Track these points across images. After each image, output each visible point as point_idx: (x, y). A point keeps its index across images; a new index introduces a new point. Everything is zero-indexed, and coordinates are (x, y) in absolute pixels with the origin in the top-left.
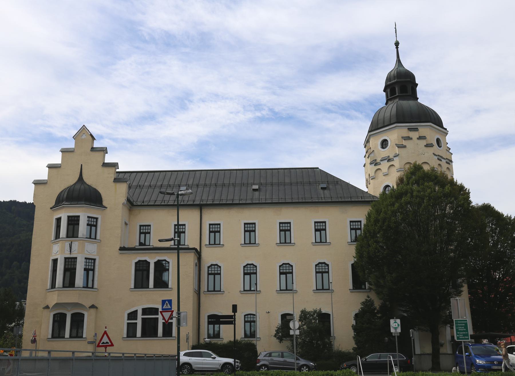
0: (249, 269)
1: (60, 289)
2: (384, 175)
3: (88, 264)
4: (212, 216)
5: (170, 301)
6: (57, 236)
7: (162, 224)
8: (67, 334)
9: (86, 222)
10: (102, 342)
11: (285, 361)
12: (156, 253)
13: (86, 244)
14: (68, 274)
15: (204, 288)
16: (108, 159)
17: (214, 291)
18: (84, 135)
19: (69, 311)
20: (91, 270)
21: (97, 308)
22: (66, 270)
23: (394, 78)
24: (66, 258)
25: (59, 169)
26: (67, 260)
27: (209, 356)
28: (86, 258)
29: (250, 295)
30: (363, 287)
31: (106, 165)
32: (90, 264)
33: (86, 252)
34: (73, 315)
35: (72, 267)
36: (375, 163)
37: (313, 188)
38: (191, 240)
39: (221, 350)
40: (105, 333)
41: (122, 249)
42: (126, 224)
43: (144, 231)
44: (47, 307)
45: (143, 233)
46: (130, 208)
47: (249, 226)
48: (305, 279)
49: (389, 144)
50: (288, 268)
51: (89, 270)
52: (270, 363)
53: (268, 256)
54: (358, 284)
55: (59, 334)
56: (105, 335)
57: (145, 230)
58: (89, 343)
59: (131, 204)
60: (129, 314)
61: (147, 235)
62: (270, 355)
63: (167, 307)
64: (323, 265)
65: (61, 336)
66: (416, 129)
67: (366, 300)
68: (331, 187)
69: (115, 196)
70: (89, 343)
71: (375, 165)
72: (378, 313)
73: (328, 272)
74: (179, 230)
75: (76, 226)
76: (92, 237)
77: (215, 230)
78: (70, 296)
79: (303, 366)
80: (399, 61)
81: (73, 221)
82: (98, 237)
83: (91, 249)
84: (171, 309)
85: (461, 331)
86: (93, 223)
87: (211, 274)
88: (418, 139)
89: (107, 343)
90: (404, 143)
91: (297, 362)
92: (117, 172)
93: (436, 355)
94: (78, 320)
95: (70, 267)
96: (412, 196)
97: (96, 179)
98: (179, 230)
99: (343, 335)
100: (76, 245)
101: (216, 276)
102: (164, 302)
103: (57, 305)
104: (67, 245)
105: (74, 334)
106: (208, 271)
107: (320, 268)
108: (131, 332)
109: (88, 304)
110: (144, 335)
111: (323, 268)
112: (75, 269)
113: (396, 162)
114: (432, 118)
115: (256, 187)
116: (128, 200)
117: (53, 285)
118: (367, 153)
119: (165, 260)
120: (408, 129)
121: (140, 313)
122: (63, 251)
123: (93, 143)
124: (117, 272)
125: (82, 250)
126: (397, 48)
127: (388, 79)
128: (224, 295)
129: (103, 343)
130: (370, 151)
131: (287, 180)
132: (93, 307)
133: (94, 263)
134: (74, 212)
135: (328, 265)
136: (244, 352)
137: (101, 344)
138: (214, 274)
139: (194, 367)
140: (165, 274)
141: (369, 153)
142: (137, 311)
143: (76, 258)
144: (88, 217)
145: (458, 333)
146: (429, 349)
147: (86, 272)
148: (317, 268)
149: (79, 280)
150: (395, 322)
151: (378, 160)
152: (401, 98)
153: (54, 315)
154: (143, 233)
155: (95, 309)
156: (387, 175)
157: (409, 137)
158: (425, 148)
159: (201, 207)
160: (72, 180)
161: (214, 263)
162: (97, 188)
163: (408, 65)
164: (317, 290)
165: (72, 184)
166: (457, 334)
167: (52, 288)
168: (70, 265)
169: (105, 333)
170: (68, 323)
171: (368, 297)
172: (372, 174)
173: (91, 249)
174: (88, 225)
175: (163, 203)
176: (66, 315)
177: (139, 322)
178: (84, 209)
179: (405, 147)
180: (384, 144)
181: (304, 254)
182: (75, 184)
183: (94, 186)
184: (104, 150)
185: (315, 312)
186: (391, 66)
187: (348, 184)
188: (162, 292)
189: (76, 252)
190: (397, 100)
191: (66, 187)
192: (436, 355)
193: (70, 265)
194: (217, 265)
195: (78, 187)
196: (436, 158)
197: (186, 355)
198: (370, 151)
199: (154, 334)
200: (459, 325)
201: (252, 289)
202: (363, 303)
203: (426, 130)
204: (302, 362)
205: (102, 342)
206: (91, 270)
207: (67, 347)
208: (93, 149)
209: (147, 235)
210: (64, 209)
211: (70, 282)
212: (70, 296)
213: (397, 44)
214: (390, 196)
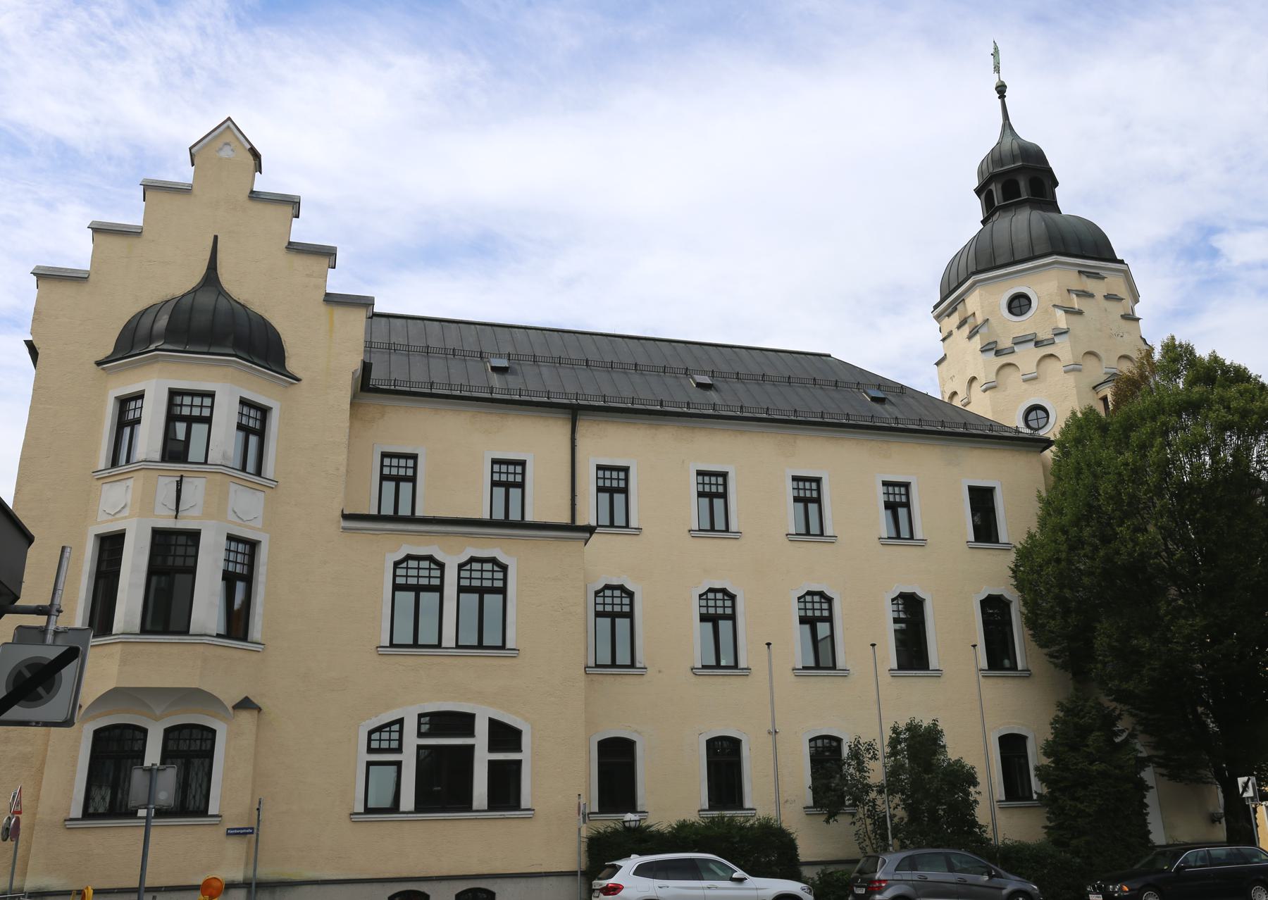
1: (132, 639)
2: (1025, 381)
4: (605, 444)
7: (457, 457)
11: (963, 883)
13: (233, 487)
18: (227, 148)
19: (157, 719)
21: (259, 709)
23: (1014, 158)
24: (156, 532)
29: (721, 680)
30: (1007, 663)
33: (232, 517)
38: (545, 500)
49: (1034, 304)
51: (239, 579)
53: (767, 570)
57: (400, 470)
58: (233, 833)
70: (233, 833)
74: (509, 476)
76: (252, 461)
77: (614, 483)
78: (166, 665)
81: (185, 412)
86: (255, 422)
94: (192, 749)
98: (509, 476)
103: (116, 696)
104: (166, 486)
109: (230, 696)
113: (1063, 348)
114: (1090, 247)
120: (1080, 272)
121: (411, 727)
124: (328, 590)
125: (216, 510)
126: (1002, 96)
128: (644, 678)
132: (246, 704)
134: (193, 374)
142: (490, 719)
147: (807, 627)
149: (207, 606)
151: (1005, 343)
153: (98, 734)
155: (256, 712)
156: (1035, 379)
158: (1123, 322)
159: (574, 412)
160: (181, 279)
162: (267, 316)
163: (1028, 133)
168: (173, 553)
173: (245, 509)
174: (701, 495)
176: (144, 731)
179: (1080, 313)
180: (1019, 304)
182: (194, 291)
183: (257, 307)
186: (988, 139)
189: (195, 512)
193: (173, 553)
199: (459, 799)
208: (254, 196)
210: (157, 366)
211: (166, 612)
212: (166, 665)
213: (1001, 90)
214: (1084, 428)
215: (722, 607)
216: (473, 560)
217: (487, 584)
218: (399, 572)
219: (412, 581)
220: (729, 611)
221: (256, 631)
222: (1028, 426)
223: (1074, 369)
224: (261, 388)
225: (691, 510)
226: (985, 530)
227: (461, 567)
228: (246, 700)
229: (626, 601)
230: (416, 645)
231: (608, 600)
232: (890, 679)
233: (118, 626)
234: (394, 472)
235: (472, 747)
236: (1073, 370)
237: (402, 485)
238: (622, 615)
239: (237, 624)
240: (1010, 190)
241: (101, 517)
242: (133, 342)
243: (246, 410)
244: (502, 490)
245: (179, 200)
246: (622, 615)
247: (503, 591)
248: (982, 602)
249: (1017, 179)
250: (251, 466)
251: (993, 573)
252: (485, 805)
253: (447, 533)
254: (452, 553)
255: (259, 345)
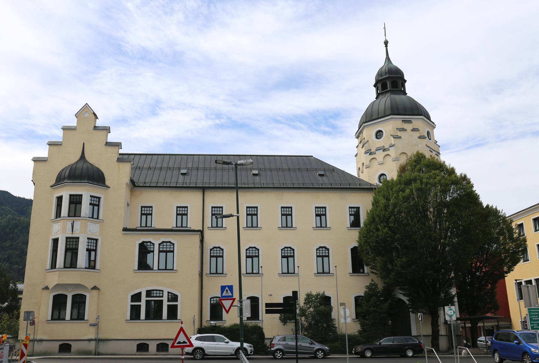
0: (251, 252)
2: (379, 164)
3: (90, 244)
5: (231, 288)
6: (58, 214)
7: (164, 207)
8: (68, 317)
9: (89, 202)
10: (177, 341)
12: (160, 234)
13: (89, 223)
14: (69, 254)
15: (206, 270)
16: (112, 138)
17: (217, 273)
19: (70, 292)
20: (93, 250)
21: (99, 289)
22: (67, 250)
23: (386, 73)
24: (67, 238)
25: (59, 147)
26: (69, 240)
27: (222, 340)
28: (88, 238)
30: (361, 270)
31: (108, 144)
32: (92, 244)
33: (88, 232)
34: (74, 297)
35: (74, 247)
36: (369, 152)
37: (309, 175)
38: (194, 222)
39: (232, 333)
40: (182, 329)
41: (125, 230)
42: (128, 205)
43: (146, 212)
44: (47, 288)
45: (144, 214)
46: (132, 188)
47: (251, 209)
48: (306, 261)
49: (384, 135)
50: (218, 252)
52: (285, 348)
53: (269, 239)
54: (357, 267)
55: (59, 316)
56: (182, 333)
57: (147, 212)
58: (91, 325)
59: (134, 184)
60: (133, 297)
61: (148, 216)
62: (284, 339)
63: (227, 295)
64: (254, 249)
65: (61, 317)
66: (410, 122)
67: (371, 284)
68: (328, 174)
69: (118, 176)
70: (91, 325)
71: (370, 154)
72: (381, 296)
73: (328, 256)
74: (182, 212)
75: (78, 205)
76: (95, 216)
78: (71, 277)
79: (318, 350)
80: (388, 58)
81: (76, 200)
82: (101, 217)
83: (93, 229)
84: (232, 296)
85: (534, 321)
86: (95, 203)
87: (214, 256)
88: (412, 130)
89: (184, 342)
90: (399, 134)
91: (312, 346)
92: (120, 154)
93: (435, 337)
94: (79, 301)
95: (71, 246)
96: (422, 183)
97: (98, 158)
98: (182, 212)
99: (345, 319)
100: (78, 224)
101: (324, 258)
102: (223, 288)
103: (58, 286)
104: (69, 224)
105: (56, 316)
106: (211, 253)
107: (215, 252)
108: (135, 313)
109: (90, 286)
110: (148, 317)
111: (254, 252)
112: (77, 249)
113: (392, 152)
114: (416, 110)
115: (256, 172)
116: (132, 181)
117: (53, 265)
118: (360, 143)
119: (150, 242)
120: (403, 121)
121: (144, 295)
122: (64, 230)
123: (95, 121)
124: (119, 252)
125: (84, 230)
126: (386, 46)
127: (380, 74)
129: (179, 343)
130: (363, 142)
131: (285, 166)
132: (95, 288)
133: (96, 243)
135: (328, 250)
136: (248, 333)
137: (176, 344)
138: (217, 257)
139: (207, 351)
140: (149, 256)
141: (363, 143)
142: (141, 292)
143: (78, 238)
144: (91, 196)
145: (532, 322)
146: (428, 330)
147: (88, 252)
148: (283, 252)
150: (451, 310)
151: (373, 150)
152: (392, 92)
153: (55, 297)
154: (144, 214)
155: (97, 290)
156: (382, 164)
157: (403, 129)
158: (419, 139)
159: (204, 189)
160: (74, 158)
161: (217, 246)
162: (99, 168)
163: (396, 62)
164: (318, 273)
165: (73, 162)
166: (531, 324)
167: (52, 268)
168: (72, 246)
169: (182, 329)
170: (68, 305)
171: (372, 281)
172: (367, 163)
173: (93, 229)
174: (91, 204)
175: (165, 185)
176: (67, 296)
177: (143, 304)
178: (86, 188)
179: (400, 137)
180: (379, 134)
181: (305, 239)
182: (77, 162)
184: (107, 130)
185: (318, 295)
186: (381, 63)
187: (343, 172)
188: (168, 274)
190: (389, 94)
191: (67, 165)
192: (435, 337)
193: (72, 246)
194: (219, 247)
195: (80, 165)
196: (428, 149)
197: (197, 339)
198: (363, 142)
200: (533, 314)
201: (254, 272)
202: (367, 287)
203: (418, 122)
204: (317, 346)
205: (177, 341)
206: (93, 250)
207: (69, 330)
208: (95, 128)
209: (148, 216)
210: (66, 188)
212: (71, 277)
213: (386, 43)
215: (324, 253)
216: (163, 242)
217: (167, 250)
218: (161, 247)
219: (165, 249)
220: (327, 254)
221: (98, 266)
222: (380, 182)
223: (396, 160)
224: (97, 191)
225: (313, 220)
226: (355, 223)
227: (160, 244)
228: (95, 286)
229: (327, 252)
230: (166, 269)
231: (286, 252)
232: (279, 277)
233: (57, 266)
234: (181, 212)
235: (162, 300)
236: (395, 160)
237: (253, 216)
238: (326, 256)
239: (92, 265)
240: (384, 87)
241: (53, 234)
242: (60, 180)
243: (93, 199)
244: (250, 216)
245: (73, 132)
246: (326, 256)
247: (173, 252)
248: (351, 249)
249: (391, 81)
250: (95, 216)
251: (352, 238)
252: (166, 318)
253: (155, 234)
254: (156, 240)
255: (96, 177)
